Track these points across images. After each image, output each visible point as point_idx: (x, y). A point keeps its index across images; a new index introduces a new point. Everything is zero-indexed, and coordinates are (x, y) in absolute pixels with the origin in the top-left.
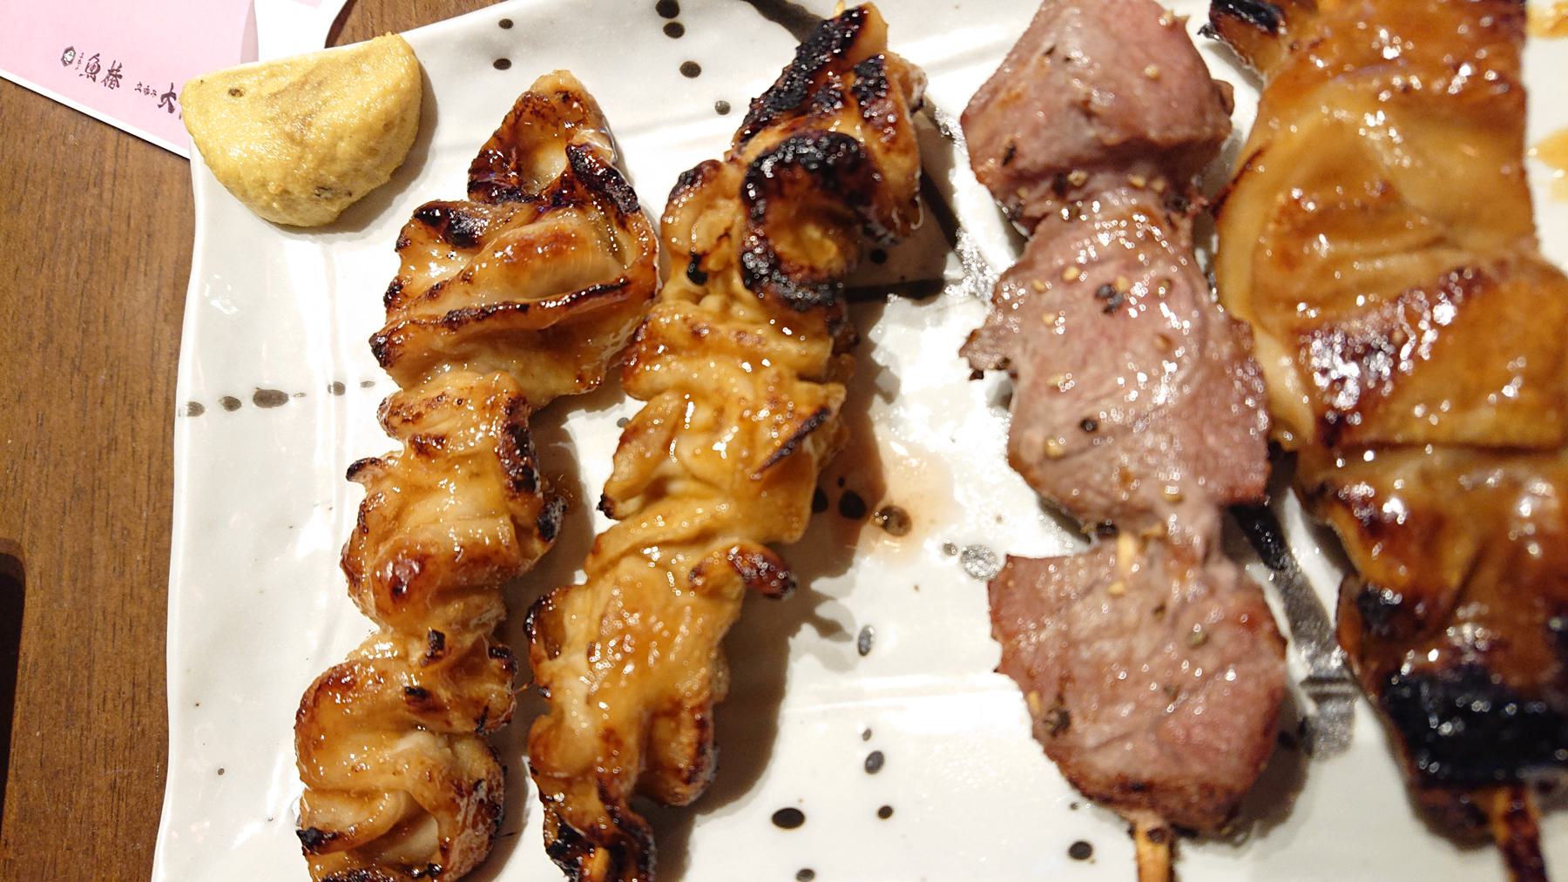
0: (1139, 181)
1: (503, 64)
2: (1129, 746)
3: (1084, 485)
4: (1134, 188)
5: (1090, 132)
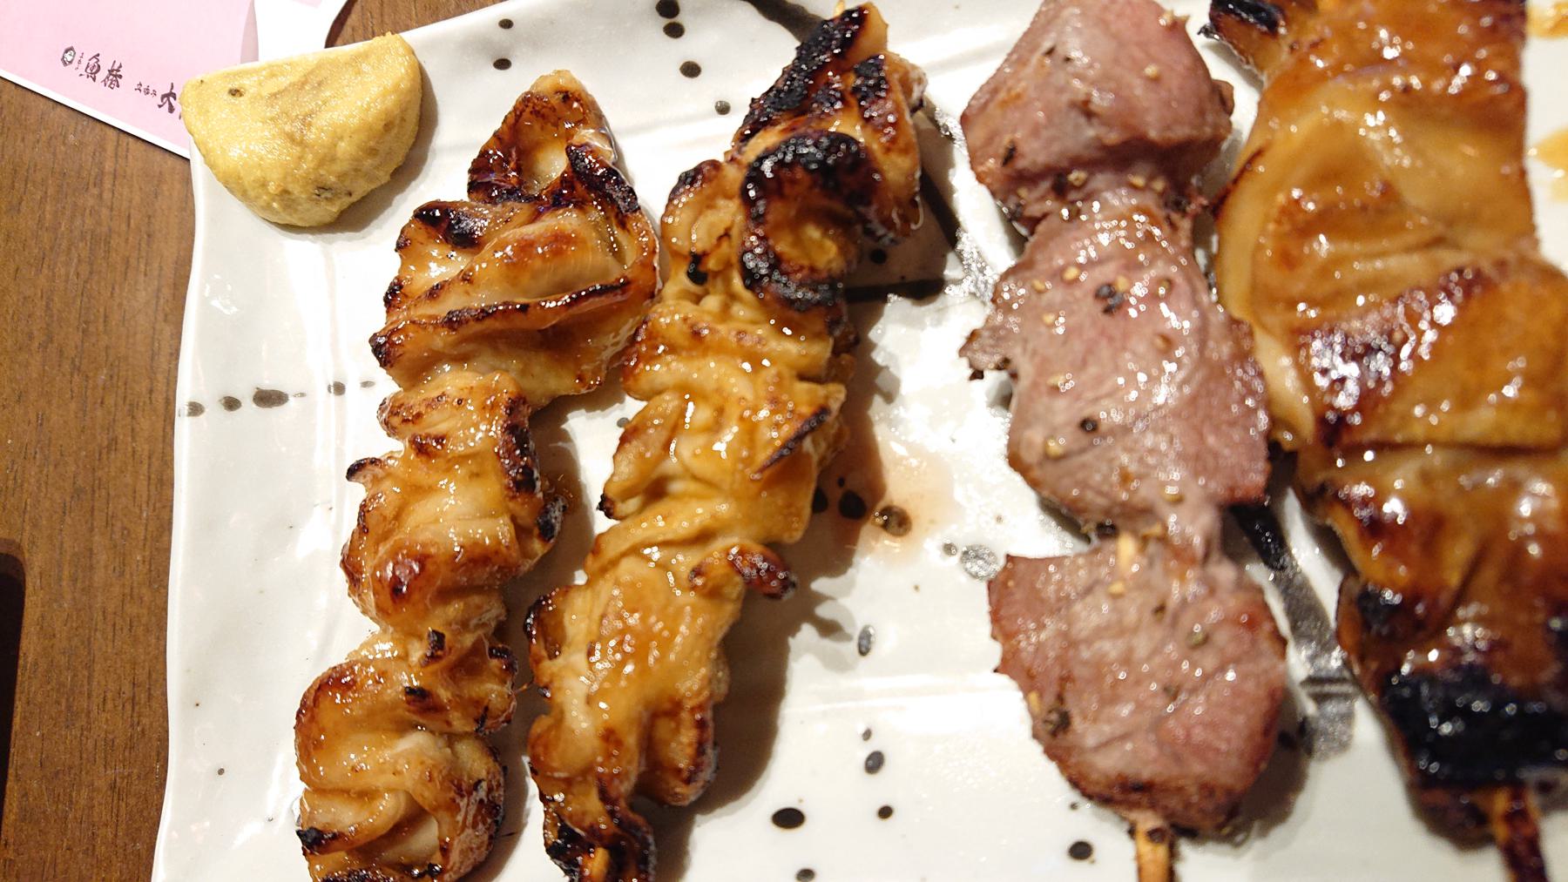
0: (1139, 181)
1: (503, 64)
2: (1129, 746)
3: (1084, 485)
4: (1134, 188)
5: (1090, 132)
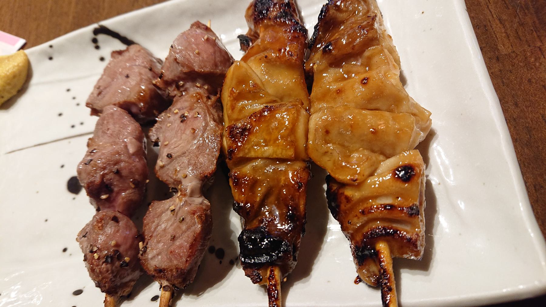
0: (198, 85)
1: (51, 58)
2: (160, 257)
3: (167, 175)
4: (198, 87)
5: (180, 68)
